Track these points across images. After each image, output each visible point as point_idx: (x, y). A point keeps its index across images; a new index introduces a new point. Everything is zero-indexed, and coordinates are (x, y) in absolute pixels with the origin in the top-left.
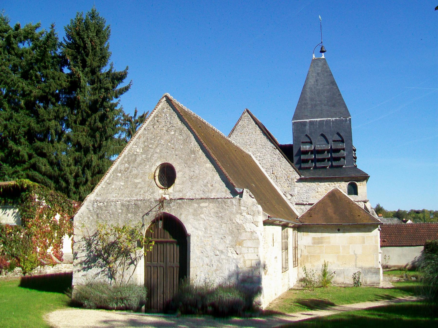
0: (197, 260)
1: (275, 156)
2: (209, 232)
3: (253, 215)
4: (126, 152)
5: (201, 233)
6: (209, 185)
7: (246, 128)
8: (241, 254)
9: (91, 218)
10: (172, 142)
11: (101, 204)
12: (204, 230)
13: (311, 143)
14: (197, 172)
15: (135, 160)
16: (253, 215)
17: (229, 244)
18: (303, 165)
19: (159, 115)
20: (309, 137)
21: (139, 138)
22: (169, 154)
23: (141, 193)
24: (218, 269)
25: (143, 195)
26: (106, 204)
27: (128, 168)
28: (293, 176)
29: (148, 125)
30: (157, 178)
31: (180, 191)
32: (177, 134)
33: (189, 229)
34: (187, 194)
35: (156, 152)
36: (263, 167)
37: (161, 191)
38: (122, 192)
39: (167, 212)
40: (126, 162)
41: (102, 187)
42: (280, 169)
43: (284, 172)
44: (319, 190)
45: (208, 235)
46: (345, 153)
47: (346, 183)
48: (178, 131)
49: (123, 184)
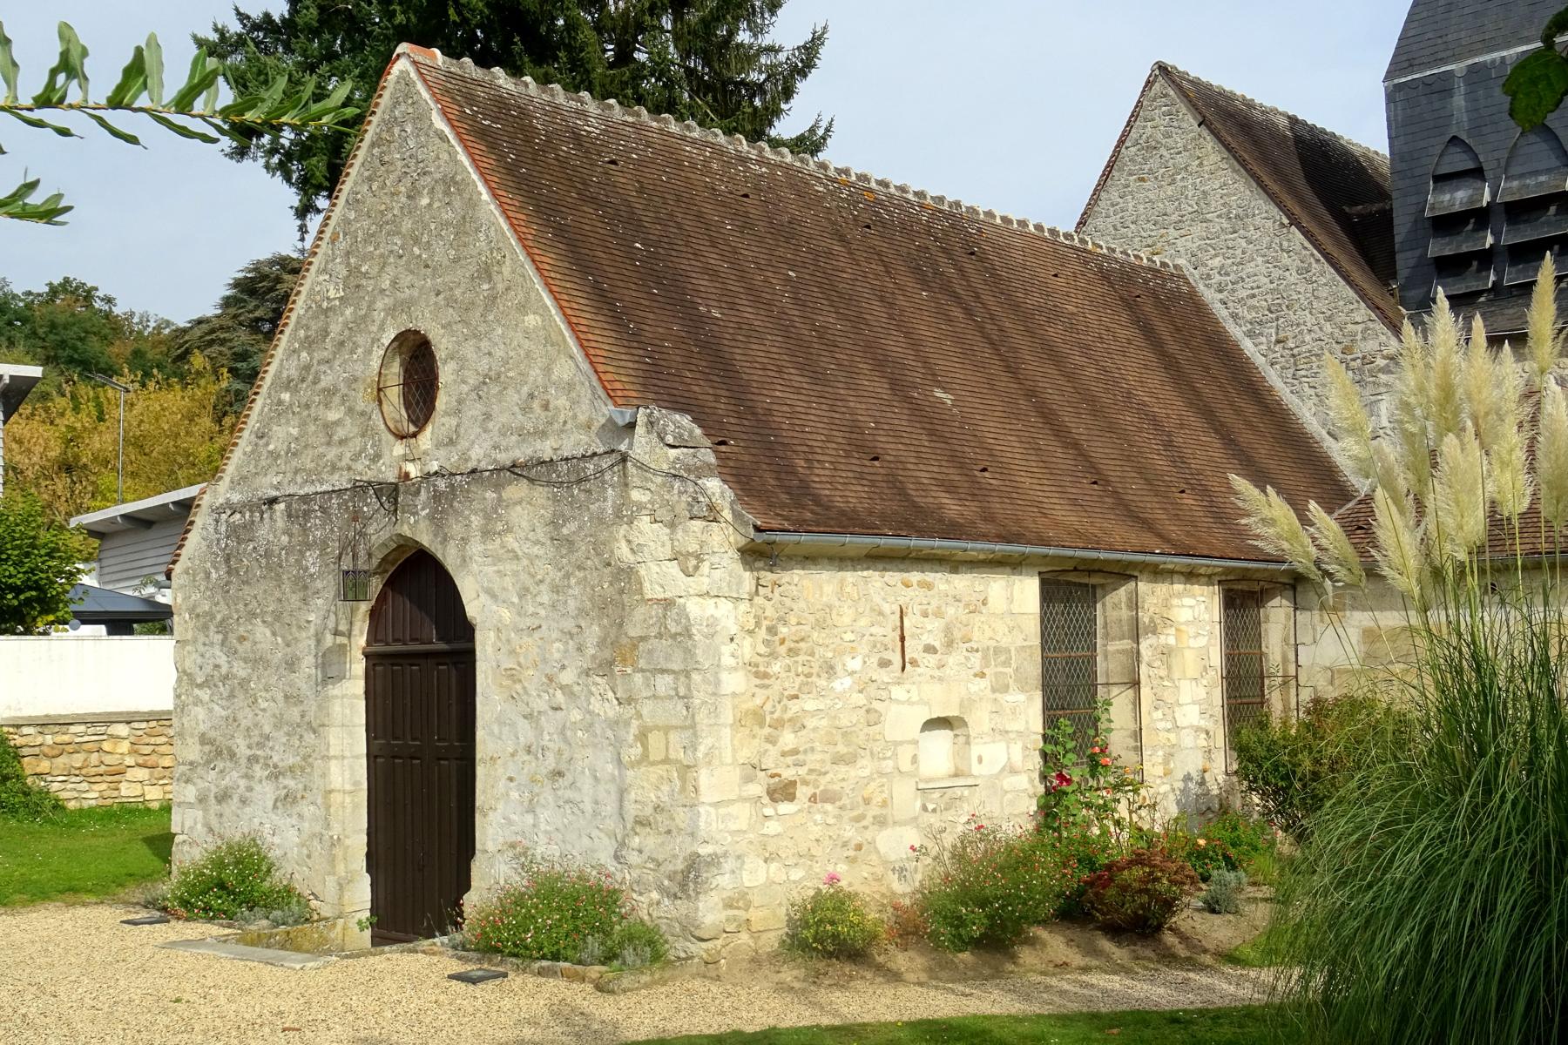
0: (496, 729)
2: (531, 610)
4: (299, 307)
6: (536, 405)
7: (1163, 151)
8: (630, 700)
12: (516, 600)
13: (1477, 173)
14: (499, 353)
15: (326, 333)
16: (672, 525)
17: (594, 657)
19: (384, 135)
24: (563, 767)
27: (307, 368)
28: (1371, 345)
29: (355, 183)
36: (1235, 316)
37: (399, 449)
39: (408, 534)
43: (1328, 327)
48: (440, 188)
49: (295, 432)
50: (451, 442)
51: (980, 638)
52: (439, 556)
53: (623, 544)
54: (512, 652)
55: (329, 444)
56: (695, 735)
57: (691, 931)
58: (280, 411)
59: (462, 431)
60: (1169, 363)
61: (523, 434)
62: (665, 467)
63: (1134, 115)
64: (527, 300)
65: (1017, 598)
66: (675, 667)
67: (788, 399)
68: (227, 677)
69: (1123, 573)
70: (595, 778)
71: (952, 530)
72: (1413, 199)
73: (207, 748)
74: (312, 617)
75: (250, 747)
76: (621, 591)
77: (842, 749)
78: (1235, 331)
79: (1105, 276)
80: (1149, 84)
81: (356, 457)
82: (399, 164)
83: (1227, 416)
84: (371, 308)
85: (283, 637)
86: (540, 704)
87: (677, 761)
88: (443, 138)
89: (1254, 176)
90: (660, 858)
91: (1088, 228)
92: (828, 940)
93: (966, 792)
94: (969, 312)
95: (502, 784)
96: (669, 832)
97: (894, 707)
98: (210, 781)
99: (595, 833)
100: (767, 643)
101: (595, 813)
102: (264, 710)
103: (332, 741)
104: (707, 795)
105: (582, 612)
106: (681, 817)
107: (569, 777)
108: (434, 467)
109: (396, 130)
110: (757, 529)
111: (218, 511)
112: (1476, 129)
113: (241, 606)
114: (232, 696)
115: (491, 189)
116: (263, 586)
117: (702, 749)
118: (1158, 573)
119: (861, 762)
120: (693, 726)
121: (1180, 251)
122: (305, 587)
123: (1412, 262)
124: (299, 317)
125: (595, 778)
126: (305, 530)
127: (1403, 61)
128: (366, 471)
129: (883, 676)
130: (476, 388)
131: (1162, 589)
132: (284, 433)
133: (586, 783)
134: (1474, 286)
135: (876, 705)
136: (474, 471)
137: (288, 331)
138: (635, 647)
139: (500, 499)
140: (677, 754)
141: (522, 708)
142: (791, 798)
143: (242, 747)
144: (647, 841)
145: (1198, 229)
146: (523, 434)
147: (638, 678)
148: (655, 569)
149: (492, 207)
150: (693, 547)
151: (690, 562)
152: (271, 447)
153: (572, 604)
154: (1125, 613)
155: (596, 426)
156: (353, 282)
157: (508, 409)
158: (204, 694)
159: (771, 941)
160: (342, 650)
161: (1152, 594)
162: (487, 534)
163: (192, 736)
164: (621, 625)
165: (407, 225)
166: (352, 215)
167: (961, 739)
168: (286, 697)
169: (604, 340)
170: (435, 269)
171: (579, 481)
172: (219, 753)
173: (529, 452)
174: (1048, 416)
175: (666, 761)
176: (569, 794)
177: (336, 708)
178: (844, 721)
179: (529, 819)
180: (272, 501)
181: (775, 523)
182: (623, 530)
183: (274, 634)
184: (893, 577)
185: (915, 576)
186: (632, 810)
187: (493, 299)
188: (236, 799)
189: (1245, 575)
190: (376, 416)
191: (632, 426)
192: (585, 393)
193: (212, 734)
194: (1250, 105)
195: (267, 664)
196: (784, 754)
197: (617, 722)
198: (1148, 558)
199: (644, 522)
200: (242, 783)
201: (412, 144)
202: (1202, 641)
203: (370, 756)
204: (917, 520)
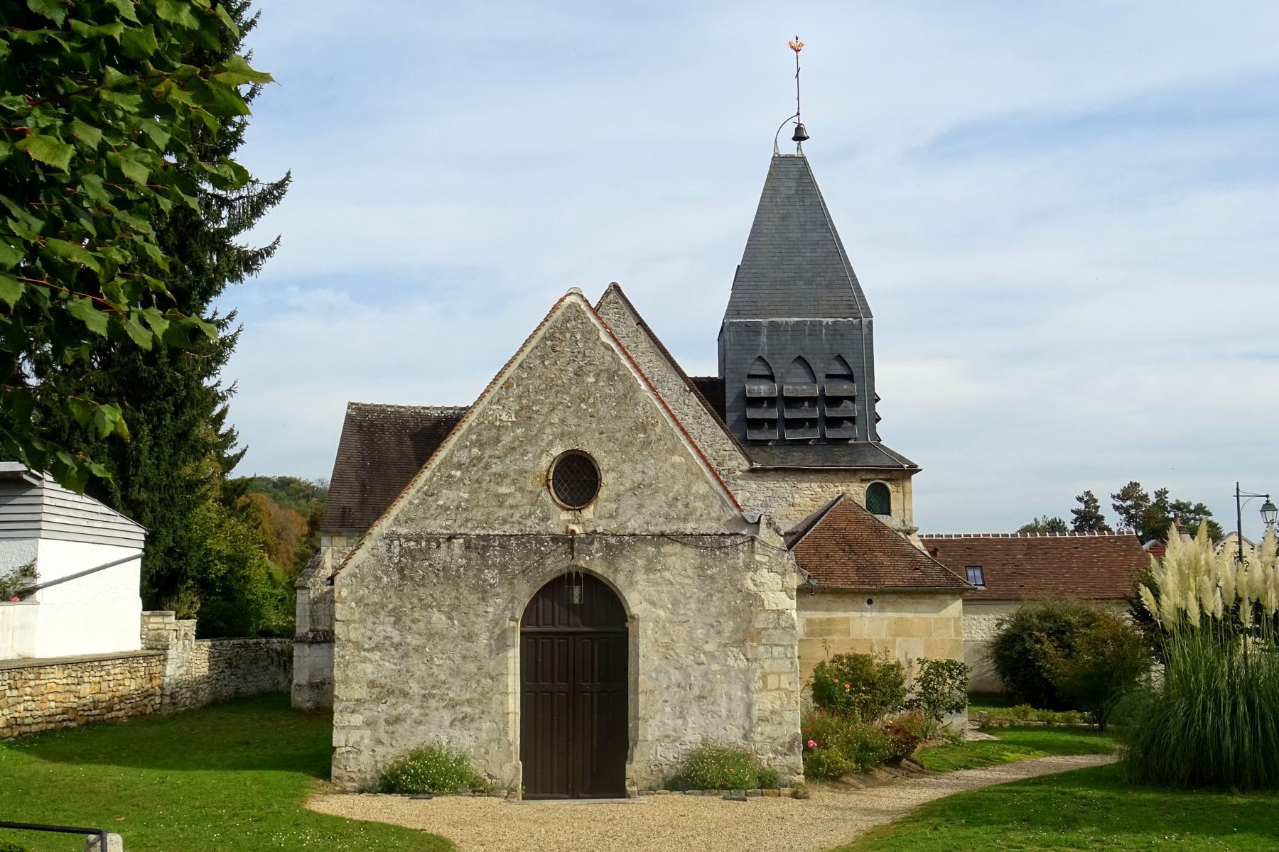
0: (654, 675)
1: (686, 409)
2: (682, 612)
3: (783, 575)
5: (662, 613)
8: (756, 660)
9: (385, 579)
10: (591, 400)
13: (771, 378)
14: (651, 473)
15: (498, 441)
16: (783, 575)
17: (730, 638)
18: (754, 435)
20: (767, 364)
21: (508, 388)
22: (582, 430)
24: (705, 694)
26: (424, 544)
27: (479, 459)
28: (734, 464)
31: (611, 516)
34: (629, 525)
35: (552, 424)
37: (565, 516)
38: (464, 515)
40: (473, 444)
41: (411, 503)
44: (798, 501)
45: (680, 618)
46: (854, 409)
48: (604, 376)
49: (466, 496)
55: (500, 506)
61: (668, 518)
73: (376, 690)
74: (490, 610)
80: (607, 294)
84: (541, 431)
105: (721, 614)
112: (771, 354)
116: (440, 588)
133: (724, 703)
137: (458, 434)
148: (771, 594)
162: (648, 570)
164: (750, 622)
173: (675, 528)
175: (779, 689)
176: (711, 707)
179: (680, 722)
182: (750, 574)
186: (756, 713)
187: (647, 444)
199: (764, 572)
201: (581, 345)
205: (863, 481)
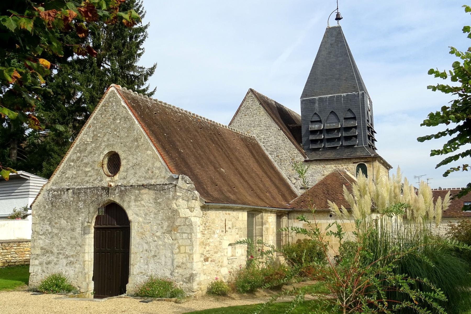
0: (137, 246)
2: (148, 218)
5: (141, 219)
6: (150, 172)
7: (251, 109)
8: (176, 239)
10: (118, 130)
11: (56, 192)
12: (144, 216)
13: (320, 121)
14: (139, 159)
15: (86, 149)
16: (188, 201)
17: (166, 230)
19: (106, 104)
20: (318, 116)
22: (115, 143)
23: (91, 181)
24: (156, 254)
25: (92, 183)
27: (79, 157)
29: (97, 114)
30: (105, 166)
32: (122, 123)
33: (131, 216)
34: (131, 181)
36: (267, 149)
37: (108, 179)
39: (112, 199)
40: (78, 151)
41: (57, 177)
42: (284, 152)
43: (288, 154)
47: (354, 165)
48: (123, 119)
49: (75, 173)
50: (124, 178)
51: (238, 226)
52: (122, 205)
53: (174, 205)
54: (142, 228)
55: (86, 176)
56: (193, 247)
57: (191, 290)
58: (70, 167)
59: (128, 176)
60: (257, 162)
62: (186, 188)
63: (244, 100)
64: (148, 147)
65: (243, 216)
66: (188, 232)
67: (197, 170)
68: (51, 233)
69: (260, 211)
70: (166, 257)
71: (234, 202)
72: (306, 126)
73: (43, 251)
74: (80, 218)
75: (58, 250)
76: (174, 215)
77: (216, 250)
78: (267, 153)
79: (242, 139)
80: (248, 93)
81: (95, 180)
82: (111, 112)
83: (269, 173)
84: (100, 144)
85: (70, 223)
86: (151, 240)
87: (188, 253)
88: (124, 107)
89: (272, 118)
90: (183, 274)
91: (231, 125)
92: (216, 291)
93: (235, 260)
94: (222, 149)
95: (139, 259)
96: (185, 268)
97: (224, 241)
98: (44, 259)
99: (165, 269)
100: (204, 227)
101: (165, 265)
102: (63, 241)
103: (86, 249)
104: (195, 260)
105: (163, 219)
106: (189, 265)
107: (158, 257)
108: (120, 184)
109: (110, 104)
110: (206, 202)
111: (49, 191)
112: (320, 112)
113: (56, 215)
114: (52, 237)
115: (139, 121)
116: (64, 210)
117: (194, 250)
118: (266, 211)
119: (219, 253)
120: (192, 245)
121: (254, 133)
122: (79, 211)
123: (306, 140)
124: (77, 144)
125: (166, 257)
126: (78, 197)
127: (305, 94)
128: (97, 183)
129: (222, 234)
130: (132, 166)
131: (267, 214)
132: (70, 173)
133: (163, 258)
134: (319, 146)
135: (221, 241)
136: (131, 186)
137: (73, 148)
138: (178, 227)
139: (140, 193)
140: (188, 251)
141: (145, 241)
142: (208, 261)
143: (55, 250)
144: (180, 271)
145: (259, 128)
146: (145, 178)
147: (178, 234)
148: (183, 210)
149: (139, 125)
150: (193, 206)
151: (191, 209)
152: (67, 176)
153: (160, 217)
154: (260, 220)
155: (166, 178)
156: (95, 138)
157: (141, 172)
158: (43, 237)
159: (204, 292)
160: (89, 226)
161: (265, 215)
162: (136, 200)
163: (38, 247)
165: (112, 126)
166: (95, 122)
167: (234, 248)
168: (71, 238)
169: (166, 157)
170: (121, 138)
171: (163, 190)
172: (47, 252)
173: (148, 182)
174: (241, 174)
175: (185, 253)
176: (158, 260)
177: (87, 241)
178: (216, 244)
179: (146, 266)
180: (68, 190)
181: (209, 201)
183: (67, 222)
184: (224, 212)
185: (227, 212)
186: (175, 264)
188: (53, 263)
189: (280, 212)
190: (101, 171)
191: (178, 178)
192: (164, 171)
193: (45, 247)
194: (267, 98)
195: (65, 230)
196: (207, 251)
197: (172, 244)
198: (265, 208)
199: (180, 200)
200: (55, 259)
201: (115, 107)
202: (273, 226)
203: (95, 252)
204: (228, 200)
205: (354, 163)
